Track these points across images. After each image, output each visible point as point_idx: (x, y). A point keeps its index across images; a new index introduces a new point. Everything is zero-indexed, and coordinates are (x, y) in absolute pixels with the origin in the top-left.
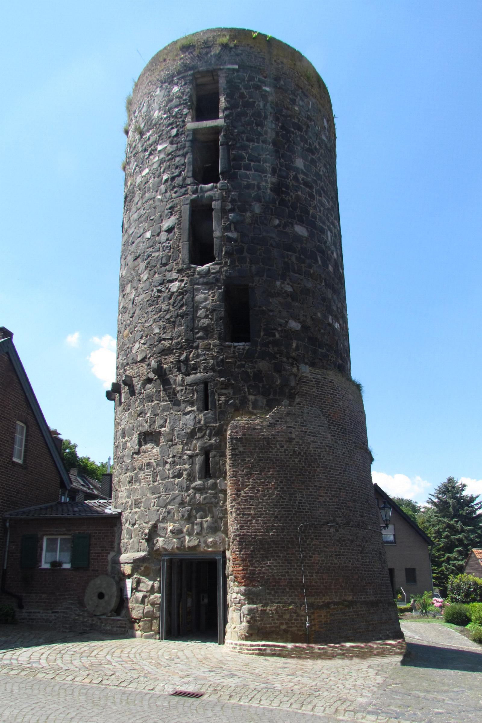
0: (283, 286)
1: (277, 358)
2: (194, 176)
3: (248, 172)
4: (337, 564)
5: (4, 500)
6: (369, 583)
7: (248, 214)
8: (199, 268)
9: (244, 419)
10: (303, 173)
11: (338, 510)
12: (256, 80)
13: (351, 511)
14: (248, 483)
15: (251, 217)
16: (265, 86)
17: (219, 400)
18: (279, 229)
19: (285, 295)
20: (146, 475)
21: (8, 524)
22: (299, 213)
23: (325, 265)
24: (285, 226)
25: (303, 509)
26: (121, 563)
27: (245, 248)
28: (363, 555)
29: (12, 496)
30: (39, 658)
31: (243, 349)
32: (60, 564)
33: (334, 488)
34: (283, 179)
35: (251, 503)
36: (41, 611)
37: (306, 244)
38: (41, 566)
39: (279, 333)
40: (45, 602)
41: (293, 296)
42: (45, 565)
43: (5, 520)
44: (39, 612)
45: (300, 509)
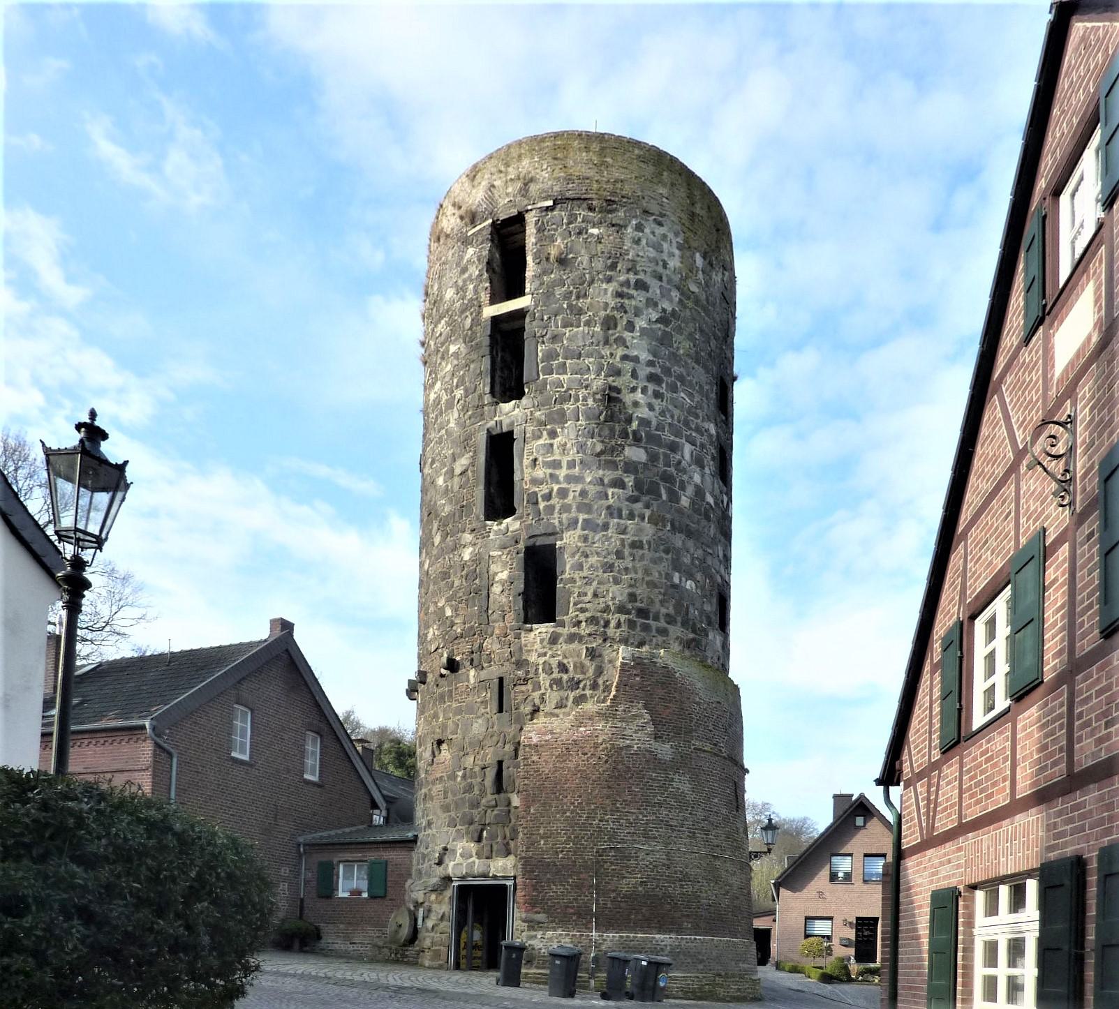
2: (492, 392)
3: (561, 377)
42: (342, 894)
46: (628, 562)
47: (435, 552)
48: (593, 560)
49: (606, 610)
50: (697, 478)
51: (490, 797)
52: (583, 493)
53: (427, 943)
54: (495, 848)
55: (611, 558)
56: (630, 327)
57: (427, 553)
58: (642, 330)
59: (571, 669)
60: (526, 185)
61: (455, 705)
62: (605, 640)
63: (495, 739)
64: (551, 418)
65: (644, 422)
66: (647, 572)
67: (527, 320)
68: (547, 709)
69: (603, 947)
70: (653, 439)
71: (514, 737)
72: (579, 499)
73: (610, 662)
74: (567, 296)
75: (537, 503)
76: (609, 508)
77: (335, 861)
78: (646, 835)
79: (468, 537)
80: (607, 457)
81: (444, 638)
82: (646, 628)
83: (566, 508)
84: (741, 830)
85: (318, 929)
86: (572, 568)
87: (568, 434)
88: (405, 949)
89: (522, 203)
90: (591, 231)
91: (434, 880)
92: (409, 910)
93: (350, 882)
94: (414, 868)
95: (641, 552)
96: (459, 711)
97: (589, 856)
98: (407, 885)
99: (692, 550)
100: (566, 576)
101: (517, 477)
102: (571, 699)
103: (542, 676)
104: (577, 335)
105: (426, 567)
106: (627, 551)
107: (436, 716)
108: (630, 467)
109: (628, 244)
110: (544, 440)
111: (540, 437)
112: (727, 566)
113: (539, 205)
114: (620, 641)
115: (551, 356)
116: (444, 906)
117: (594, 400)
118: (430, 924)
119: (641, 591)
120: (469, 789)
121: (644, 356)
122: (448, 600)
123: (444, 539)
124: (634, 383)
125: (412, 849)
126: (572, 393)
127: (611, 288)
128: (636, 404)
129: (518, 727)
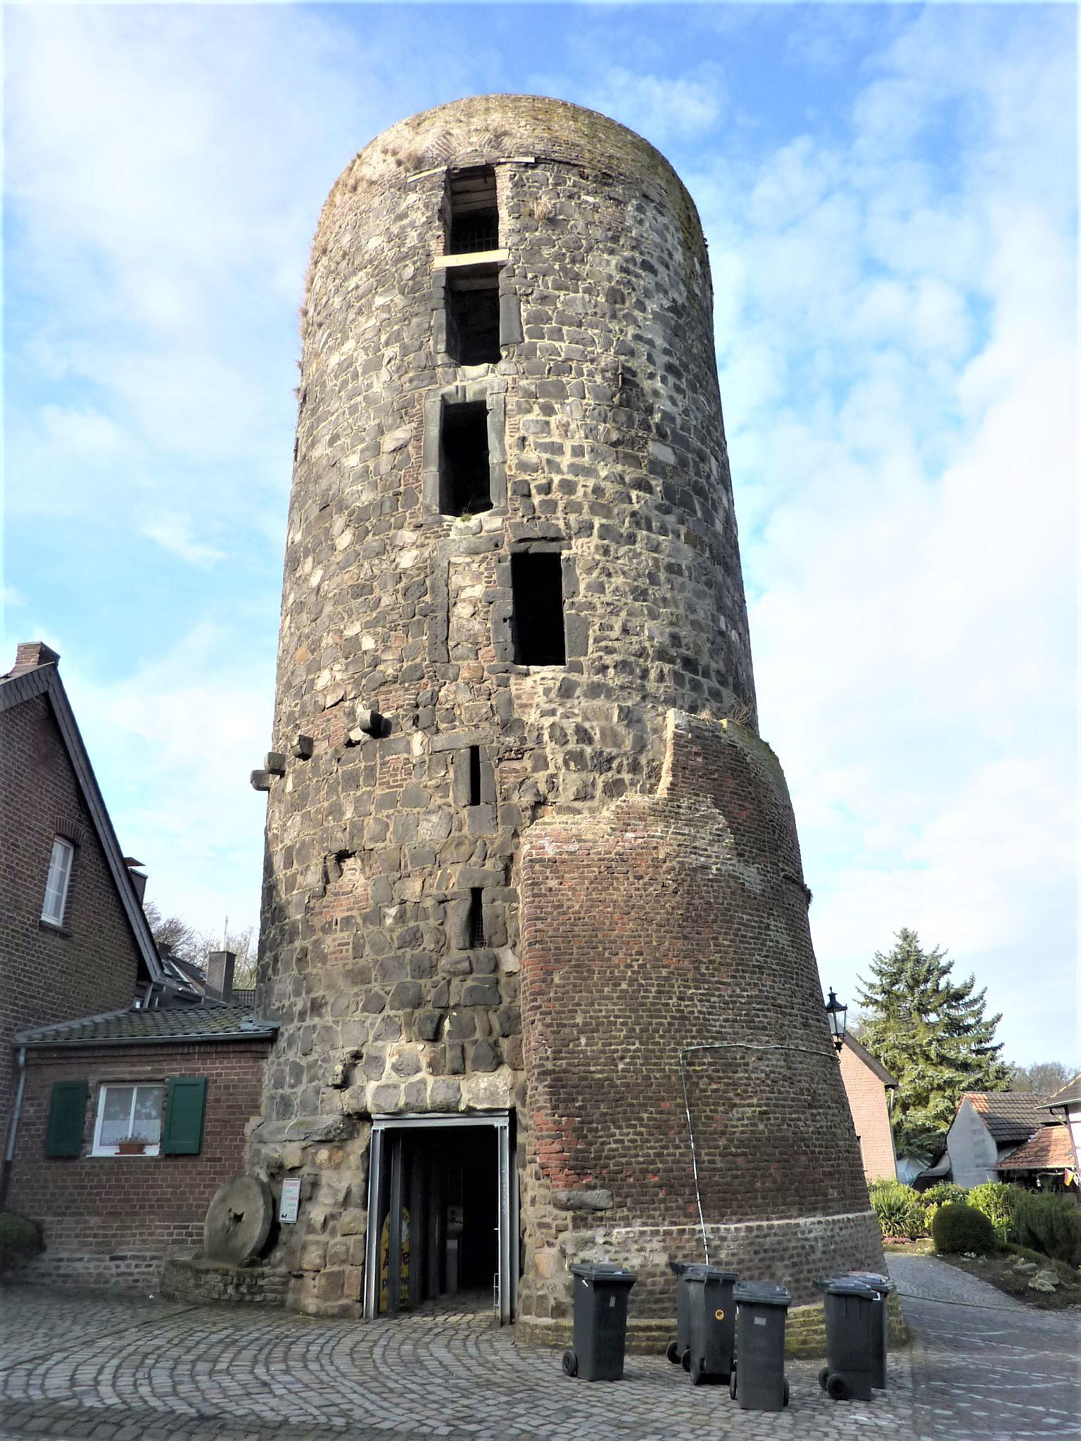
2: (449, 351)
3: (557, 344)
6: (830, 1173)
20: (340, 945)
21: (22, 1059)
23: (709, 519)
26: (867, 1190)
28: (815, 1111)
29: (35, 997)
30: (96, 1378)
32: (140, 1146)
33: (748, 966)
36: (87, 1256)
38: (90, 1152)
40: (95, 1236)
42: (100, 1149)
43: (16, 1050)
44: (81, 1259)
46: (664, 590)
48: (618, 580)
49: (642, 653)
51: (456, 954)
52: (598, 491)
53: (312, 1257)
54: (470, 1052)
55: (643, 582)
56: (641, 306)
58: (654, 313)
59: (597, 737)
60: (497, 137)
61: (379, 791)
62: (644, 698)
63: (465, 849)
64: (543, 390)
65: (666, 416)
66: (691, 609)
67: (502, 275)
68: (561, 800)
69: (723, 1255)
70: (683, 442)
71: (503, 846)
72: (592, 497)
73: (655, 731)
74: (560, 257)
75: (529, 495)
76: (634, 514)
78: (750, 1024)
79: (408, 536)
80: (625, 448)
81: (357, 683)
82: (696, 687)
83: (572, 507)
85: (39, 1228)
86: (588, 588)
87: (569, 413)
88: (253, 1276)
89: (489, 154)
90: (584, 197)
91: (329, 1120)
92: (262, 1184)
93: (122, 1125)
94: (265, 1094)
95: (680, 580)
96: (389, 802)
97: (671, 1064)
98: (248, 1129)
100: (580, 599)
101: (494, 458)
102: (600, 785)
103: (550, 748)
104: (573, 300)
106: (662, 576)
107: (336, 811)
108: (656, 467)
109: (629, 222)
110: (536, 414)
111: (529, 411)
113: (516, 160)
114: (666, 702)
115: (538, 318)
116: (345, 1174)
117: (604, 378)
118: (317, 1214)
119: (685, 632)
120: (414, 938)
121: (660, 342)
122: (367, 626)
124: (651, 369)
125: (263, 1056)
126: (574, 364)
127: (614, 260)
128: (656, 393)
129: (511, 829)
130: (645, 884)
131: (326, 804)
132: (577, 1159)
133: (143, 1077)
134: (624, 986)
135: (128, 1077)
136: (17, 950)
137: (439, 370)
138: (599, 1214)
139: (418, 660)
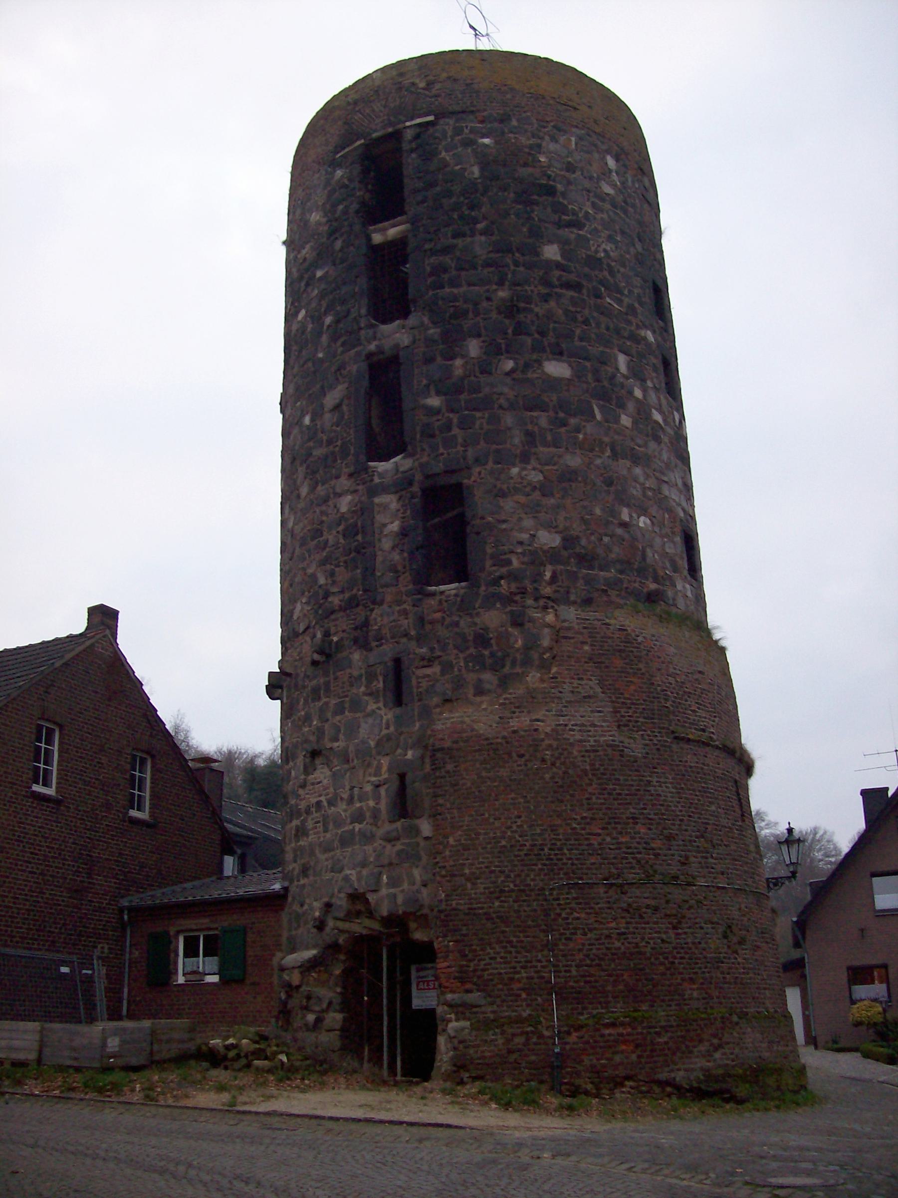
0: (524, 473)
1: (516, 602)
3: (455, 291)
4: (619, 948)
5: (118, 879)
7: (458, 362)
8: (382, 466)
9: (457, 715)
10: (558, 265)
11: (629, 856)
12: (466, 131)
13: (657, 855)
14: (461, 824)
15: (463, 366)
16: (483, 137)
17: (418, 687)
18: (515, 376)
19: (527, 489)
21: (126, 917)
22: (553, 340)
24: (527, 366)
25: (558, 860)
27: (455, 421)
31: (456, 595)
34: (519, 288)
35: (465, 857)
37: (568, 390)
39: (518, 558)
41: (544, 489)
45: (551, 859)
47: (301, 505)
50: (638, 393)
57: (291, 509)
77: (172, 931)
84: (752, 848)
99: (642, 479)
105: (290, 525)
112: (690, 497)
123: (313, 488)
130: (527, 761)
131: (303, 713)
132: (460, 972)
133: (203, 927)
134: (503, 843)
135: (195, 927)
136: (113, 840)
137: (363, 332)
138: (475, 1010)
139: (354, 591)
